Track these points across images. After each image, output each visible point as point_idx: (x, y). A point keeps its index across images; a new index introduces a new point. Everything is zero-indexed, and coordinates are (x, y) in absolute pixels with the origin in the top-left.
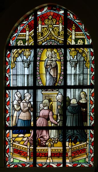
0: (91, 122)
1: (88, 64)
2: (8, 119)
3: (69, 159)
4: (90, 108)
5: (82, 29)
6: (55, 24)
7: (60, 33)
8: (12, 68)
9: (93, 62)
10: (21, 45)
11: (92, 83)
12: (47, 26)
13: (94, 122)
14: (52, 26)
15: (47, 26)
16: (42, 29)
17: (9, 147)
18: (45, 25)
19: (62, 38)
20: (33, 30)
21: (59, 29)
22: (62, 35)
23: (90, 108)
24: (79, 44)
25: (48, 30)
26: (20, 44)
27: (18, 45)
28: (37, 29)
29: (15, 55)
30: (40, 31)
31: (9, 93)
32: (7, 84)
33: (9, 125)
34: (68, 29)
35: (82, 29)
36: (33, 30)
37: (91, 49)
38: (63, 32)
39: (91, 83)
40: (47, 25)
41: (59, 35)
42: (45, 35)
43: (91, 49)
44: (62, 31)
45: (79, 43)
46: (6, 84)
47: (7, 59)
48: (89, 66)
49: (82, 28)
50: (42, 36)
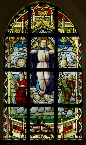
0: (79, 101)
1: (75, 50)
2: (6, 98)
3: (61, 135)
4: (79, 75)
5: (48, 8)
6: (47, 16)
7: (51, 23)
8: (10, 53)
9: (80, 48)
10: (19, 33)
11: (80, 82)
12: (40, 17)
13: (82, 101)
14: (44, 16)
15: (40, 17)
16: (35, 19)
17: (7, 124)
18: (38, 16)
19: (53, 27)
20: (27, 21)
21: (50, 20)
22: (53, 24)
23: (79, 75)
24: (68, 33)
25: (41, 20)
26: (17, 32)
27: (16, 33)
28: (31, 18)
29: (13, 42)
30: (33, 21)
31: (8, 74)
32: (6, 66)
33: (7, 102)
34: (58, 21)
35: (48, 8)
36: (27, 21)
37: (79, 108)
38: (54, 22)
39: (79, 66)
40: (40, 16)
41: (50, 25)
42: (38, 24)
43: (79, 108)
44: (53, 21)
45: (68, 31)
46: (4, 66)
47: (6, 44)
48: (76, 51)
49: (48, 7)
50: (35, 25)
